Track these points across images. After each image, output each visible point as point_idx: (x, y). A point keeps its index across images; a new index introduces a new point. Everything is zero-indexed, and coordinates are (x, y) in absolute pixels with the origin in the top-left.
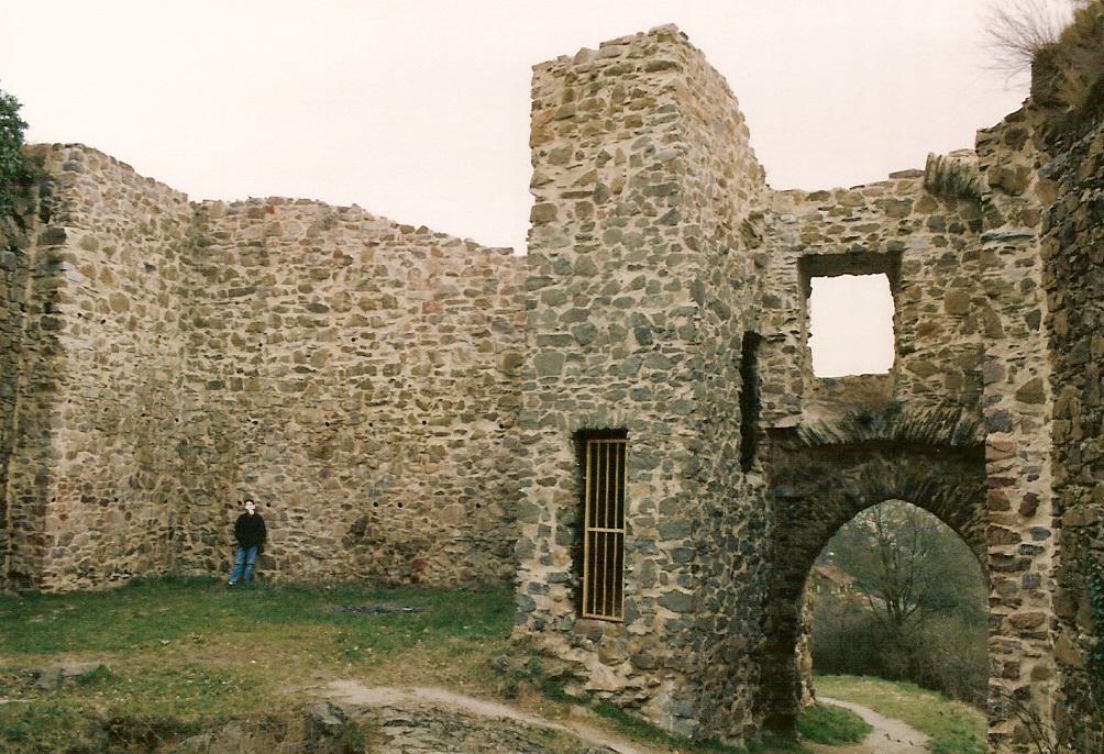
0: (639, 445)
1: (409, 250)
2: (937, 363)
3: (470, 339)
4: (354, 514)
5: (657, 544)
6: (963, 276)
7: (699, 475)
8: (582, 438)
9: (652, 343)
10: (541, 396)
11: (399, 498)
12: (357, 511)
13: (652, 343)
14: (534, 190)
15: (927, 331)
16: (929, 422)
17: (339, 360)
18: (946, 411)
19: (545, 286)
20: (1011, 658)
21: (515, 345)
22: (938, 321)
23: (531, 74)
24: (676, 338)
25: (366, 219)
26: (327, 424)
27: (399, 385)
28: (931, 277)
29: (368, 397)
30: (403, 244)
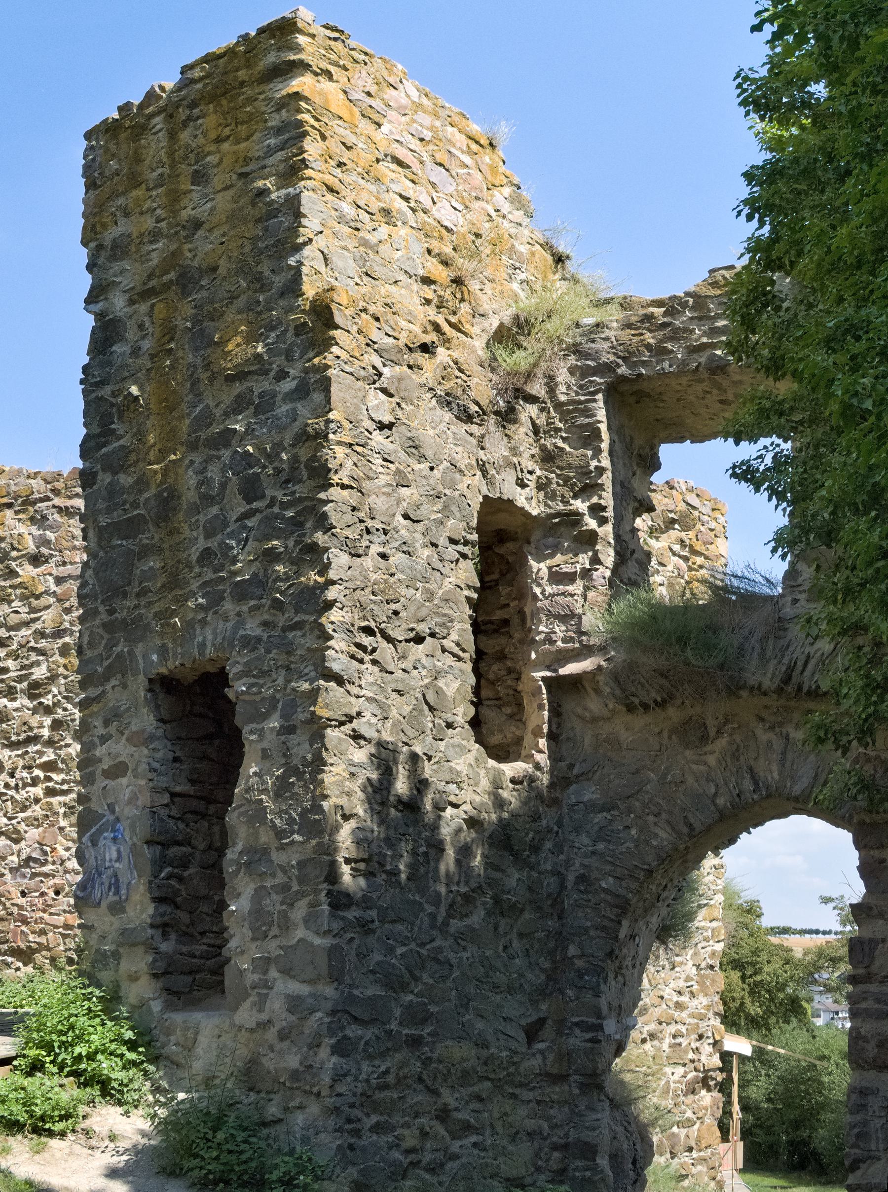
0: (245, 680)
5: (275, 856)
7: (355, 724)
9: (263, 496)
13: (263, 496)
14: (92, 307)
19: (104, 445)
23: (84, 144)
24: (300, 481)
27: (48, 710)
30: (48, 499)
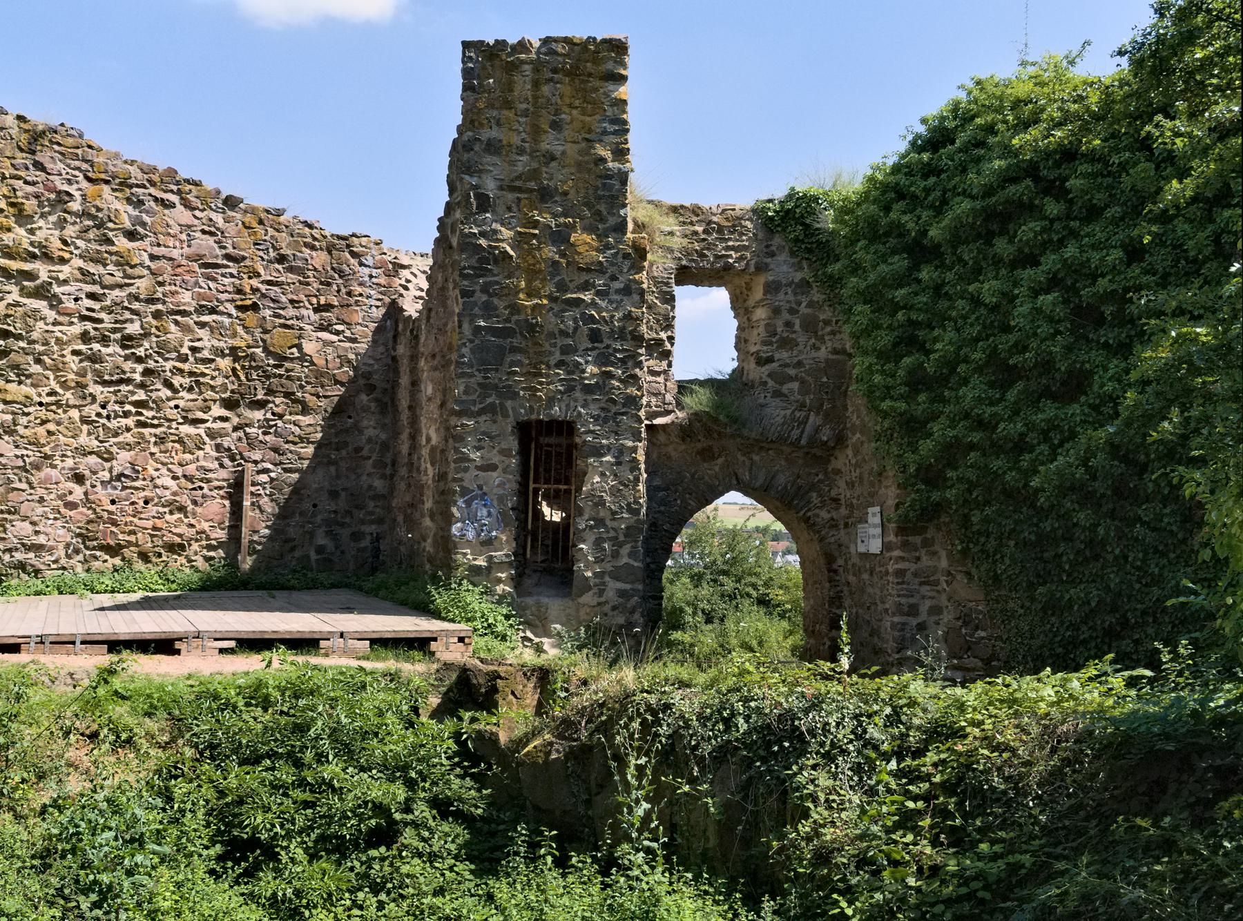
1: (150, 195)
2: (792, 372)
3: (234, 312)
4: (81, 513)
6: (815, 299)
8: (527, 432)
10: (479, 384)
11: (145, 493)
12: (85, 510)
15: (785, 343)
16: (783, 424)
17: (54, 324)
18: (798, 414)
20: (912, 601)
21: (289, 323)
22: (794, 336)
25: (90, 147)
26: (41, 404)
28: (791, 297)
29: (98, 374)
